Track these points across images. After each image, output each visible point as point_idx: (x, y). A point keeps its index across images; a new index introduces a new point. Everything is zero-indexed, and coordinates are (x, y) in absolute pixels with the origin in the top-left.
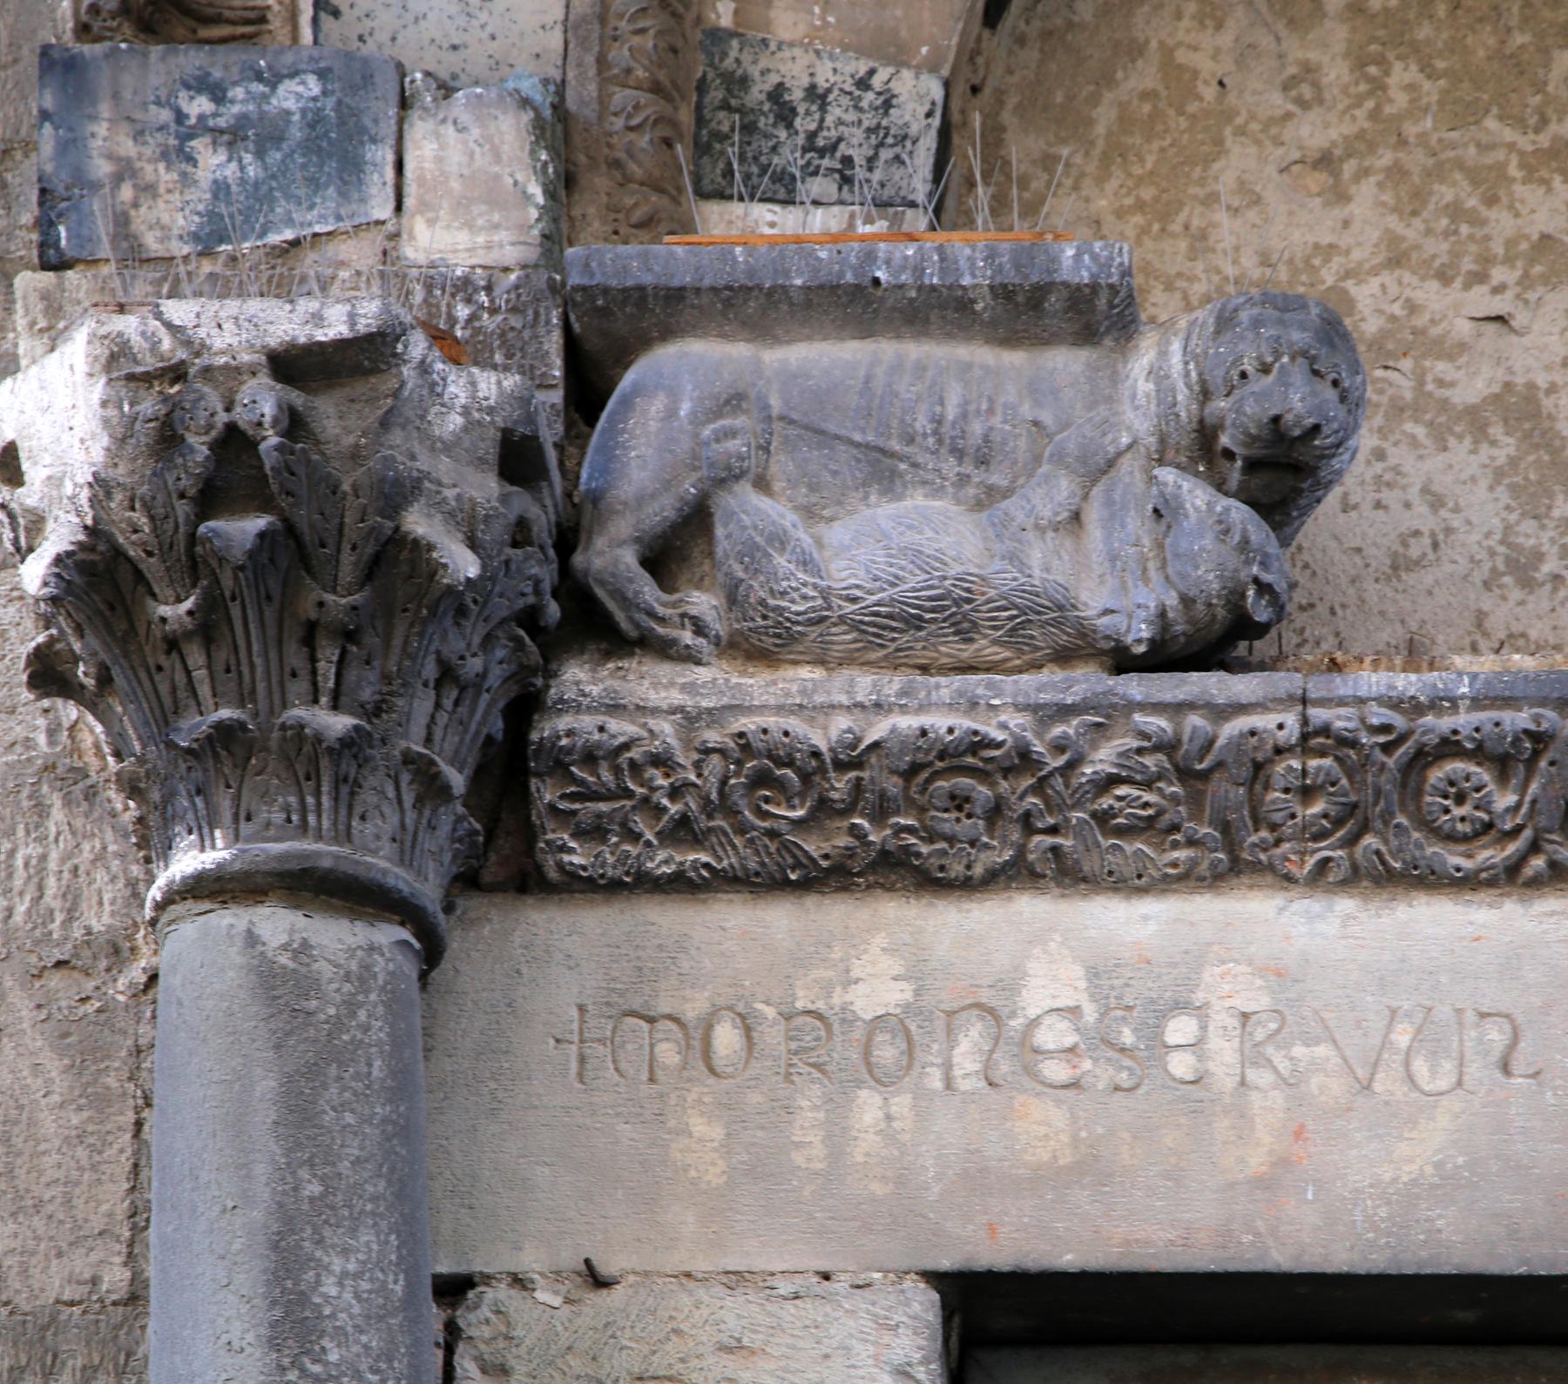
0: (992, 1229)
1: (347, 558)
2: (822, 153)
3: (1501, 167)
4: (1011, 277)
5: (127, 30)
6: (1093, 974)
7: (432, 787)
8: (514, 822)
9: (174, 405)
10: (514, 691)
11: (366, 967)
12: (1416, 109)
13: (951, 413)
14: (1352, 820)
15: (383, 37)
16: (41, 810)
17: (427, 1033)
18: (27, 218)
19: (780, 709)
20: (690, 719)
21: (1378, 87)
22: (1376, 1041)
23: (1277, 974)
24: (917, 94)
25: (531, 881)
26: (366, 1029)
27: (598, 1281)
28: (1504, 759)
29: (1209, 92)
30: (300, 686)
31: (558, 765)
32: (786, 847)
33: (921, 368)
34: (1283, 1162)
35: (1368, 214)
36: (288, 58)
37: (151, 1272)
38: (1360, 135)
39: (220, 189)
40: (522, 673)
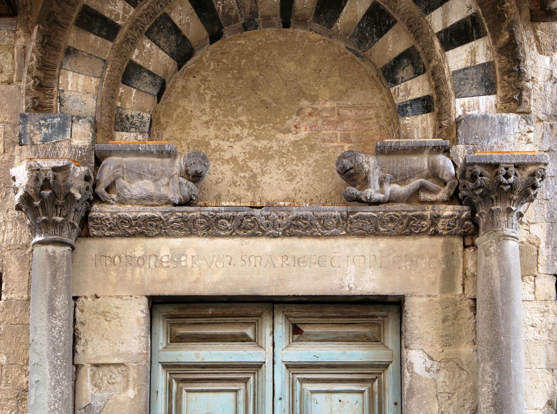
0: (155, 289)
1: (62, 196)
2: (133, 125)
3: (231, 124)
4: (158, 149)
5: (33, 110)
6: (171, 250)
7: (74, 227)
8: (86, 228)
9: (38, 174)
10: (86, 210)
11: (63, 254)
12: (219, 115)
13: (150, 168)
14: (208, 228)
15: (70, 109)
16: (16, 224)
17: (72, 259)
18: (17, 136)
19: (125, 212)
20: (112, 213)
21: (214, 112)
22: (211, 260)
23: (197, 250)
24: (147, 116)
25: (88, 236)
26: (63, 263)
27: (97, 297)
28: (229, 219)
29: (190, 113)
30: (55, 213)
31: (92, 219)
32: (126, 231)
33: (146, 162)
34: (198, 279)
35: (212, 131)
36: (56, 115)
37: (31, 295)
38: (211, 119)
39: (45, 134)
40: (87, 208)
